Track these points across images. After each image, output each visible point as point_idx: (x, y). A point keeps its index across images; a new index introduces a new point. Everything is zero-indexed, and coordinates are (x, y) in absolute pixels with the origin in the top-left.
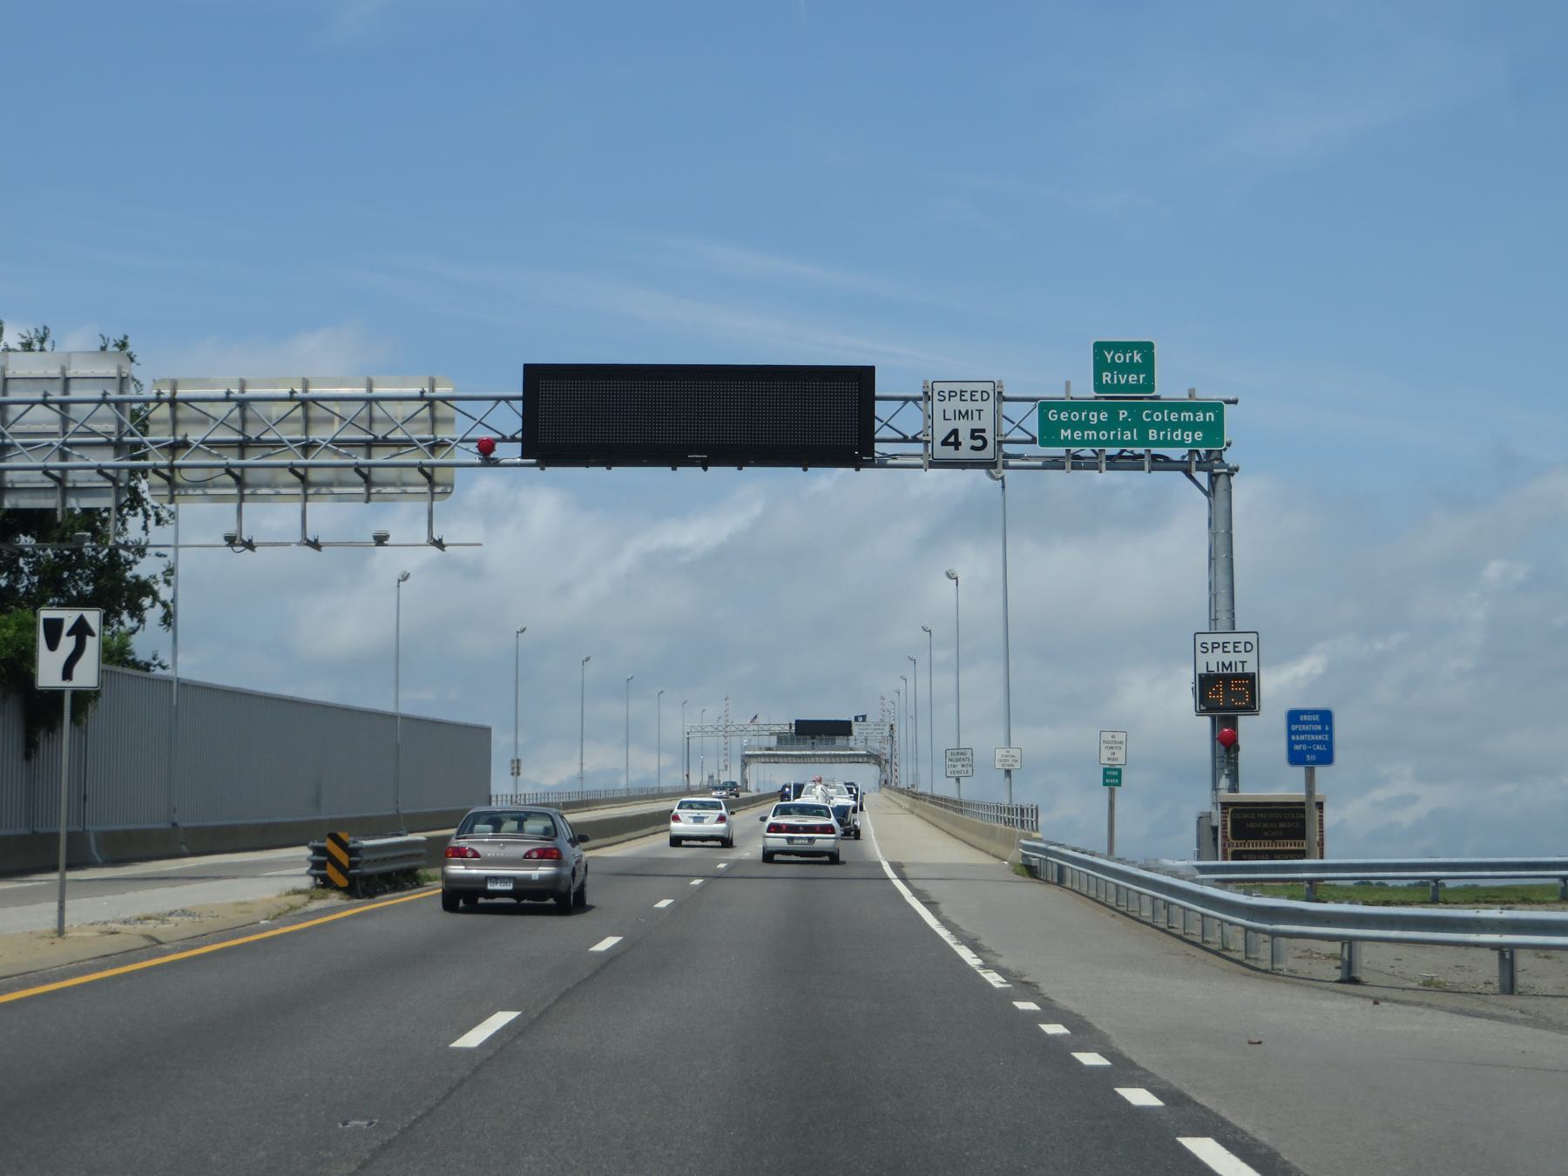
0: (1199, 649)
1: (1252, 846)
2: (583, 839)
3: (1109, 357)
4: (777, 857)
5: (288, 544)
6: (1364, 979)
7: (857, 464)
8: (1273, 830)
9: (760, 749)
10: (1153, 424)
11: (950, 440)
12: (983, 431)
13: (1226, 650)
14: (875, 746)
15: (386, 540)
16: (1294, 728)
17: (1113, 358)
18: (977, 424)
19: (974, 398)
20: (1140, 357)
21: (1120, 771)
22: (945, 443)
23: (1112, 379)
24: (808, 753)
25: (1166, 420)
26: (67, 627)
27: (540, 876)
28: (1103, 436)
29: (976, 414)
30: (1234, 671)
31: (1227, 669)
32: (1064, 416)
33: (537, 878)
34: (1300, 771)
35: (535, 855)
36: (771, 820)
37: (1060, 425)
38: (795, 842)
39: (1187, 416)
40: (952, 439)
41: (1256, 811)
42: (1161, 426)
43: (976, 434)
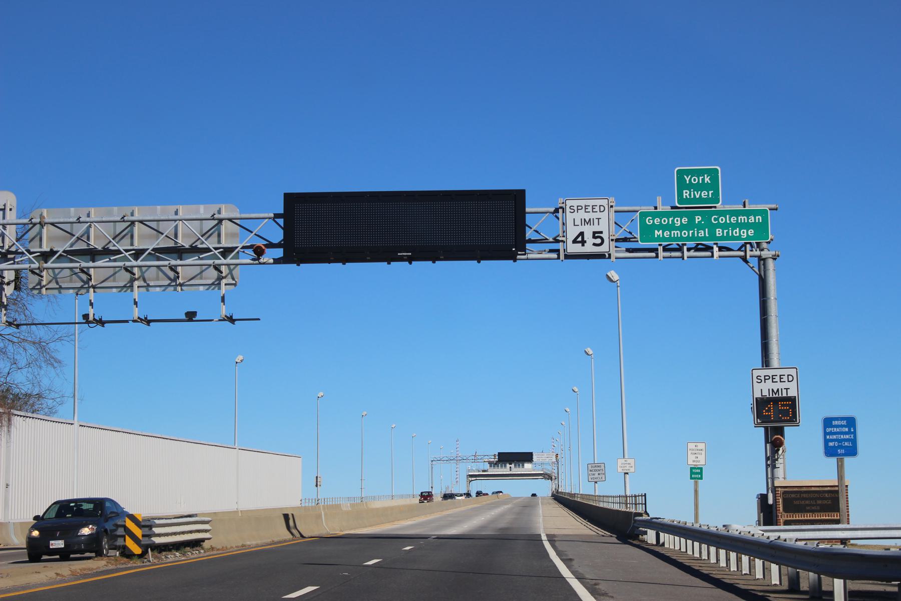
0: (755, 380)
1: (798, 517)
3: (688, 180)
5: (127, 321)
6: (13, 429)
8: (814, 505)
9: (479, 471)
10: (719, 226)
11: (578, 240)
12: (601, 232)
13: (774, 380)
14: (549, 469)
15: (195, 317)
16: (828, 430)
17: (690, 180)
18: (597, 228)
19: (594, 210)
20: (709, 179)
21: (701, 469)
22: (575, 241)
23: (690, 195)
25: (728, 222)
28: (685, 233)
29: (596, 221)
30: (780, 395)
31: (776, 394)
32: (657, 221)
34: (834, 460)
37: (654, 227)
39: (742, 219)
40: (580, 239)
41: (801, 492)
42: (724, 226)
43: (596, 235)
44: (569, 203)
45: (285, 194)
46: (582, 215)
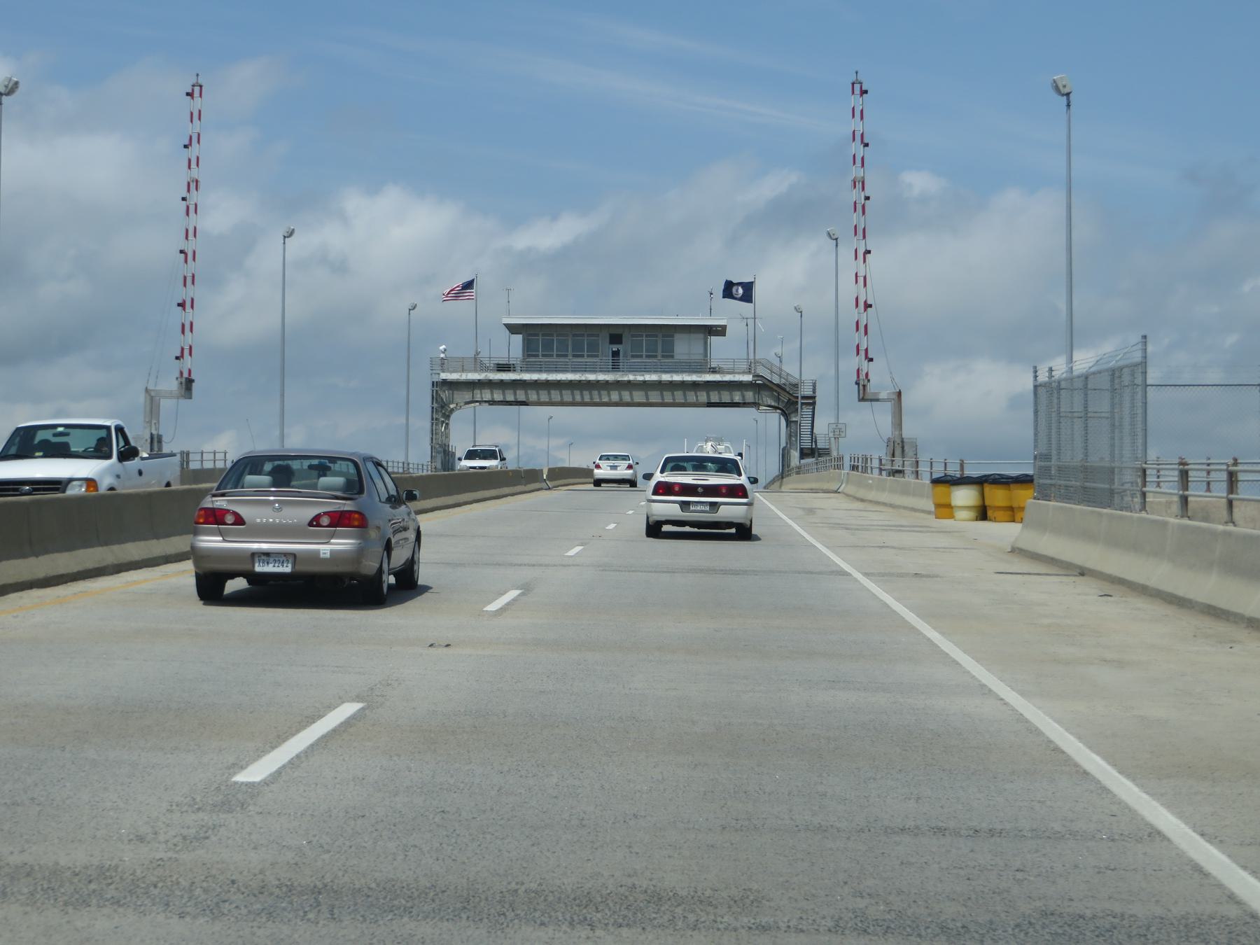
2: (411, 497)
4: (666, 528)
24: (602, 377)
27: (332, 552)
33: (328, 556)
35: (325, 521)
36: (659, 477)
38: (692, 508)
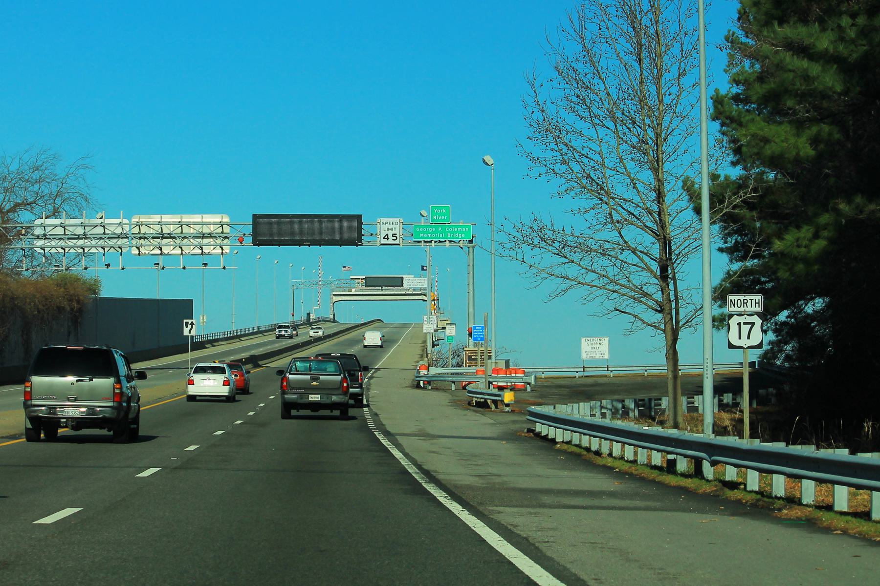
3: (436, 211)
7: (357, 245)
12: (396, 234)
22: (384, 238)
26: (189, 323)
44: (382, 221)
45: (192, 301)
46: (388, 226)
